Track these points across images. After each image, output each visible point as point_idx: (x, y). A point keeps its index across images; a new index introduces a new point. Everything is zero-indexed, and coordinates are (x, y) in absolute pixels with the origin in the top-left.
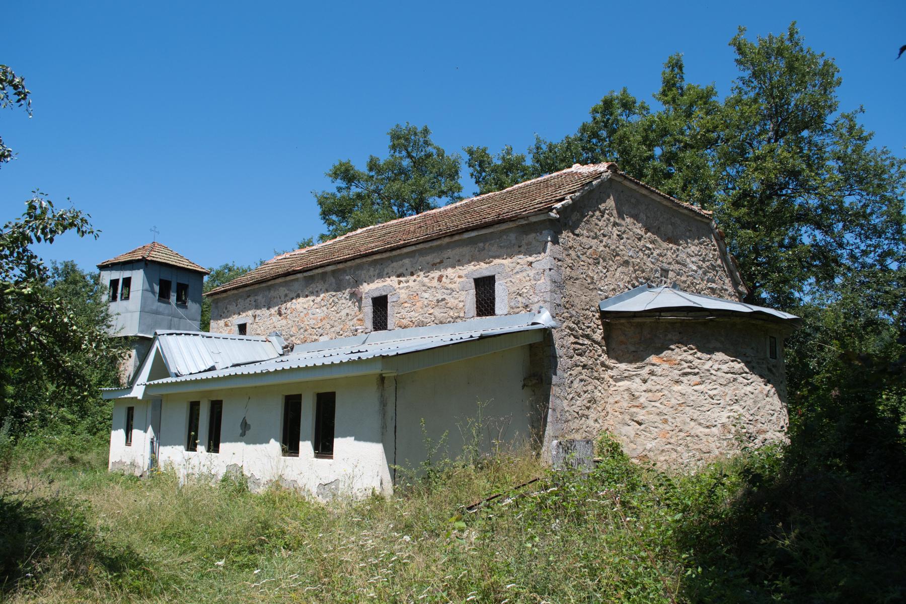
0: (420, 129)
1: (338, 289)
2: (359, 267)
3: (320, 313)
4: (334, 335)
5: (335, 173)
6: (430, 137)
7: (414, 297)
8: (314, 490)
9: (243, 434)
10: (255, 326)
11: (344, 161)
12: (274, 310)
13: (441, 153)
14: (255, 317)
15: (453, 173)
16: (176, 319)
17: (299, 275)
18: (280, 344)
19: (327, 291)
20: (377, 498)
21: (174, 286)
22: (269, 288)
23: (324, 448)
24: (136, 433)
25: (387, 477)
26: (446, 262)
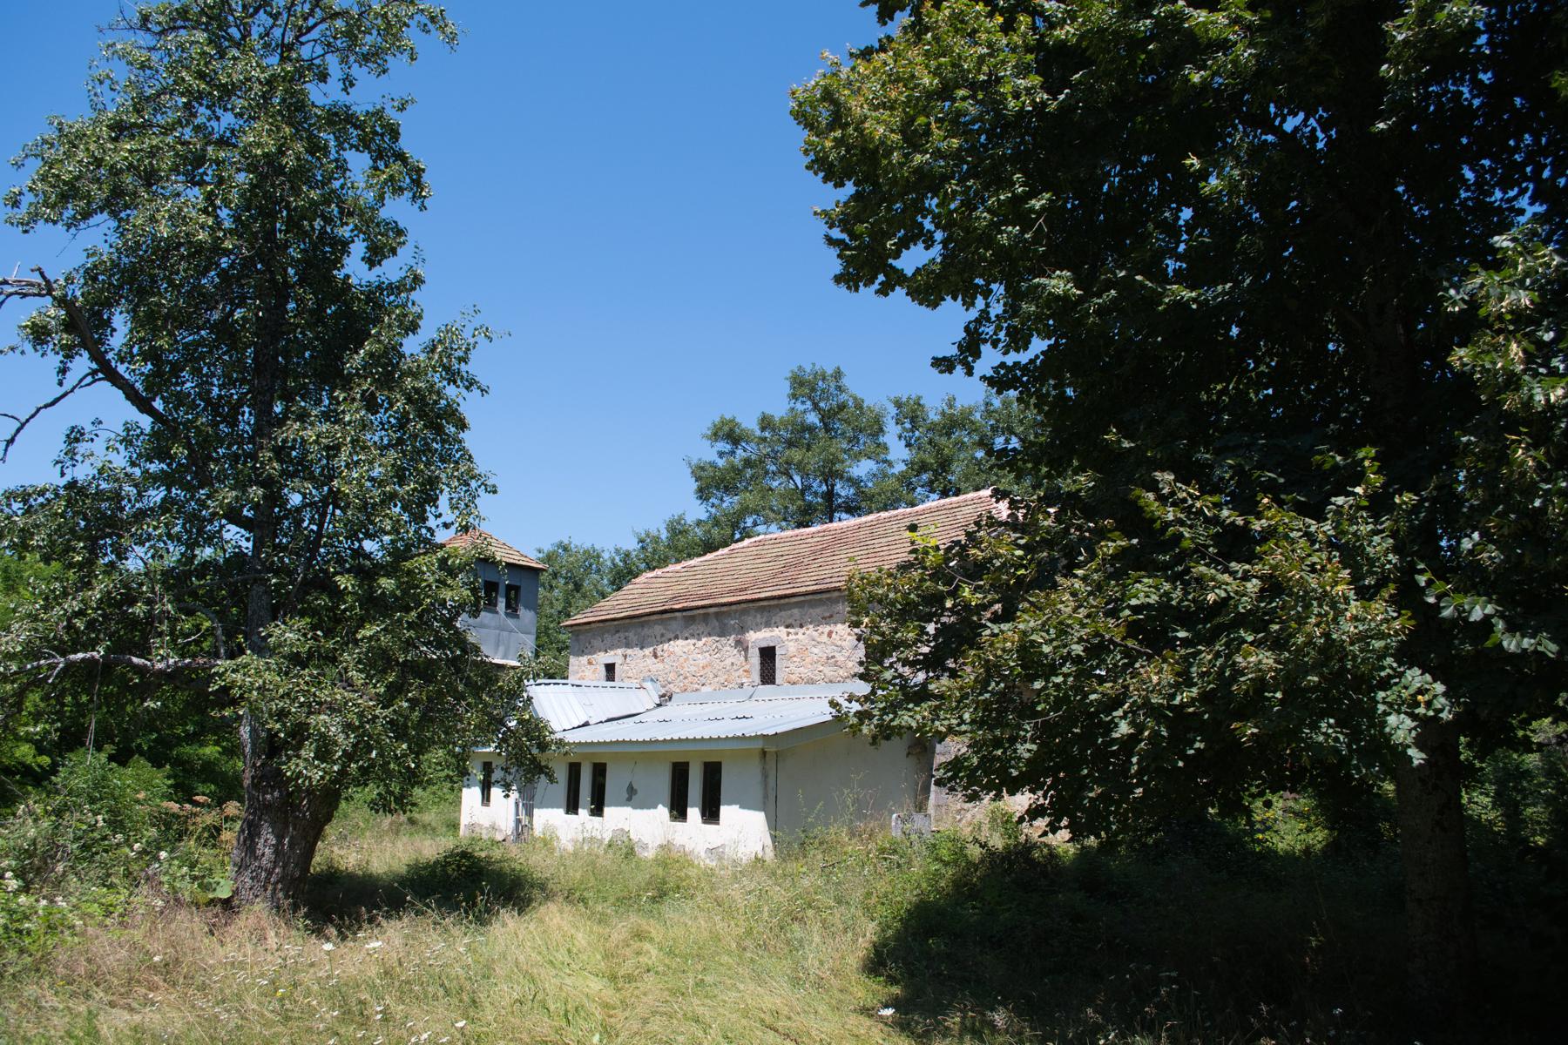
0: (830, 371)
1: (722, 634)
2: (745, 612)
3: (702, 659)
4: (718, 686)
5: (715, 434)
6: (845, 381)
7: (803, 650)
8: (703, 855)
9: (629, 799)
10: (625, 667)
11: (728, 417)
12: (648, 651)
13: (859, 405)
14: (625, 656)
15: (877, 429)
16: (505, 634)
17: (677, 614)
18: (657, 691)
19: (710, 635)
20: (759, 861)
21: (502, 589)
22: (642, 625)
23: (711, 814)
24: (496, 792)
25: (769, 842)
26: (836, 617)
